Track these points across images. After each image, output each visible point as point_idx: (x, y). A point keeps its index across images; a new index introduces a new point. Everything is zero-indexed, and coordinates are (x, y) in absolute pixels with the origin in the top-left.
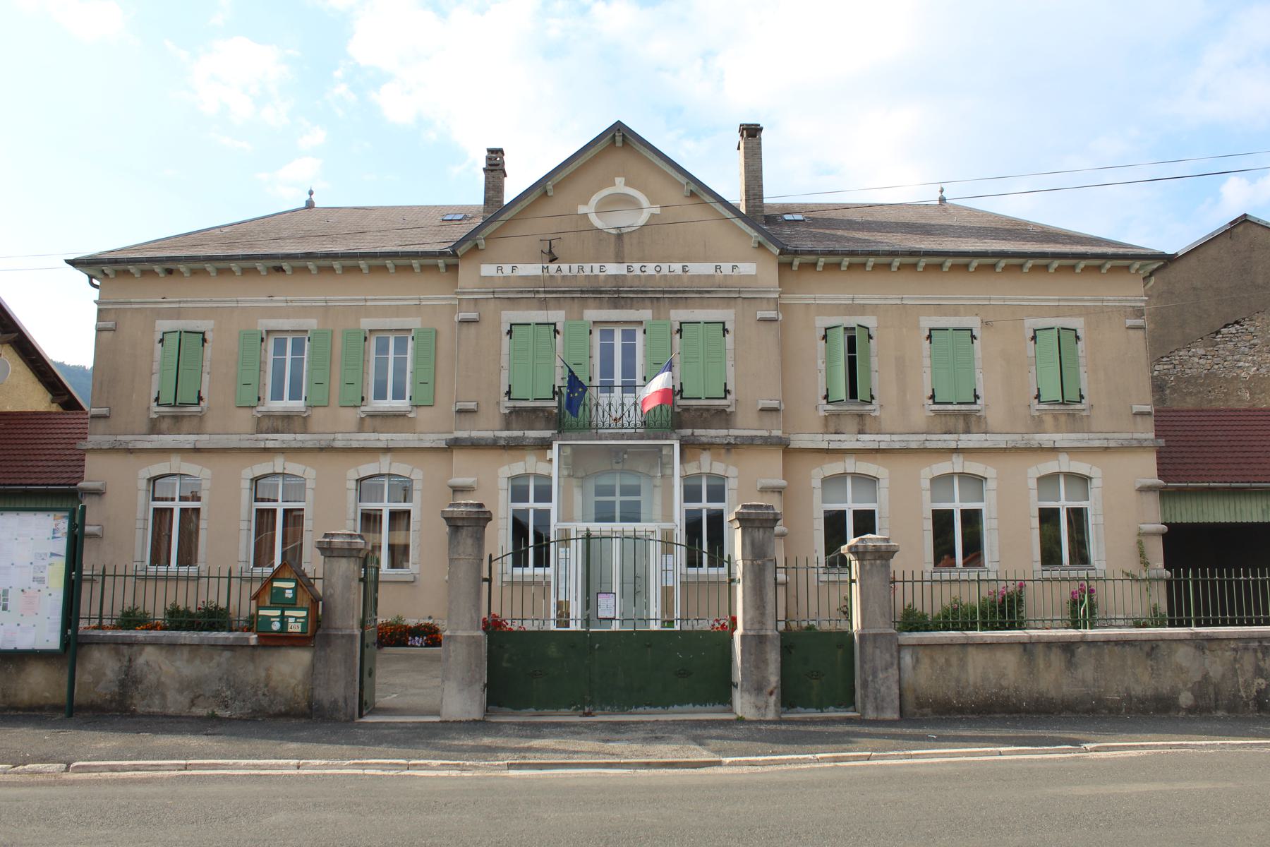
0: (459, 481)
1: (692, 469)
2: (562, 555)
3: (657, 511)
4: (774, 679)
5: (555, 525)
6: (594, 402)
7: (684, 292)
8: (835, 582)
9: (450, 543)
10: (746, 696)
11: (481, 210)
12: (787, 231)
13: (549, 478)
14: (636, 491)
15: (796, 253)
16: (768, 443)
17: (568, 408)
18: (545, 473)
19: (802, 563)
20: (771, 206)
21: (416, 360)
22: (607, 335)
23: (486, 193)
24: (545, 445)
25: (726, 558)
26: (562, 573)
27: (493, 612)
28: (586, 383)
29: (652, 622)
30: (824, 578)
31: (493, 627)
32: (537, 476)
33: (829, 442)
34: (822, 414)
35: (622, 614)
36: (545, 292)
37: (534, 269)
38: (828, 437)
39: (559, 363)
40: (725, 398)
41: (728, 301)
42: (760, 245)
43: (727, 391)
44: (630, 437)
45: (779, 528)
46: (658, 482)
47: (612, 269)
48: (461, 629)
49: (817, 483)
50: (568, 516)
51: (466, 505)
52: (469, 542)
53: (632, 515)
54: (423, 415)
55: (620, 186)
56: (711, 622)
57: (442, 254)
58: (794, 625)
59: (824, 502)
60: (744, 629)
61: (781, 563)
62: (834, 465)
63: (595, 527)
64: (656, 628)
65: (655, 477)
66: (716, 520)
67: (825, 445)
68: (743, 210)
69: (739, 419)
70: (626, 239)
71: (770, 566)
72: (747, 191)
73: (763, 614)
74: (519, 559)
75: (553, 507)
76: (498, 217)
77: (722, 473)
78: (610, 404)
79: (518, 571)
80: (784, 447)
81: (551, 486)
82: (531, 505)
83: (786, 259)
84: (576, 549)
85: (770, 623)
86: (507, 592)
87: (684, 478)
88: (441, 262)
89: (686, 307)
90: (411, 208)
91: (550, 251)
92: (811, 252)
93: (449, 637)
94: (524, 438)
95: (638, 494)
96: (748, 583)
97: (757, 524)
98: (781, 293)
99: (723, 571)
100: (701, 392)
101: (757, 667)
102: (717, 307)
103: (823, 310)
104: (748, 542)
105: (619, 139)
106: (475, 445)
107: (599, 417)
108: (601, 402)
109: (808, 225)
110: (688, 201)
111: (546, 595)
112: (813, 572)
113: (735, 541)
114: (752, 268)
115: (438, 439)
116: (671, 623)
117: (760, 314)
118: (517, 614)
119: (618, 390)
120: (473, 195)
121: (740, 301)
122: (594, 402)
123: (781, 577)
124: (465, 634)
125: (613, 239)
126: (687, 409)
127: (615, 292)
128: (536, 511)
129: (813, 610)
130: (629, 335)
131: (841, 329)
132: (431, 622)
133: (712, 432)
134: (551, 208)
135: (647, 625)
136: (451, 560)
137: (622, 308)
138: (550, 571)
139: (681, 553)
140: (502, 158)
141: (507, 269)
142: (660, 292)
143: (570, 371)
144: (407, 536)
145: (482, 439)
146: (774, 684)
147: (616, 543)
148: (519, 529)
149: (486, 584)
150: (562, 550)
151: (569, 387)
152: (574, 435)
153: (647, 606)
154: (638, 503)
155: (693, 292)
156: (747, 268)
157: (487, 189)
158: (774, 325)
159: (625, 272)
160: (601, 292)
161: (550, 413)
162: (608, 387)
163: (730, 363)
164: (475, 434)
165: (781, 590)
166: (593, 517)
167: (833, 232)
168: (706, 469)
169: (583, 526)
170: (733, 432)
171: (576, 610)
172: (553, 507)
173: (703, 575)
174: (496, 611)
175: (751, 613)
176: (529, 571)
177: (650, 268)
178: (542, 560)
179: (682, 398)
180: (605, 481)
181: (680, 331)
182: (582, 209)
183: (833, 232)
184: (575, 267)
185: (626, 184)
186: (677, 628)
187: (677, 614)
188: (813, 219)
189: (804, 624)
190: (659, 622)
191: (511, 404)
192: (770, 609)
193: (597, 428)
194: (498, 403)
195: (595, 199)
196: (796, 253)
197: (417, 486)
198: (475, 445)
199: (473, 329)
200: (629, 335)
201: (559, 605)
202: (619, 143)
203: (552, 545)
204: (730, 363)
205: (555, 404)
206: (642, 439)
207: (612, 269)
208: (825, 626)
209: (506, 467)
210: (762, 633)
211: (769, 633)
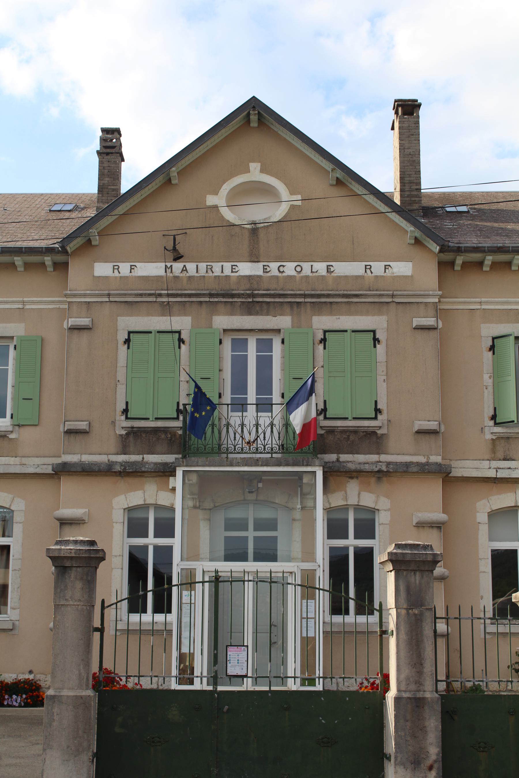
0: (67, 512)
1: (337, 500)
2: (186, 599)
3: (297, 549)
4: (434, 751)
5: (178, 565)
6: (224, 422)
7: (328, 296)
8: (504, 634)
9: (56, 588)
10: (401, 770)
11: (95, 199)
12: (448, 224)
13: (172, 509)
14: (272, 525)
15: (459, 250)
16: (425, 470)
17: (194, 428)
18: (167, 503)
19: (466, 613)
20: (431, 196)
21: (19, 372)
22: (240, 345)
23: (99, 179)
24: (168, 471)
25: (376, 606)
26: (185, 620)
27: (105, 666)
28: (215, 400)
29: (290, 681)
30: (492, 629)
31: (104, 683)
32: (158, 507)
33: (497, 469)
34: (489, 436)
35: (255, 670)
36: (168, 295)
37: (154, 269)
38: (495, 464)
39: (184, 377)
40: (376, 418)
41: (379, 306)
42: (417, 242)
43: (378, 411)
44: (266, 463)
45: (439, 570)
46: (297, 515)
47: (246, 269)
48: (68, 687)
49: (482, 517)
50: (194, 555)
51: (76, 542)
52: (79, 585)
53: (267, 553)
54: (27, 436)
55: (255, 173)
56: (359, 680)
57: (49, 250)
58: (456, 685)
59: (491, 539)
60: (399, 690)
61: (441, 612)
62: (503, 496)
63: (226, 567)
64: (294, 688)
65: (293, 509)
66: (365, 557)
67: (492, 474)
68: (397, 200)
69: (392, 443)
70: (262, 235)
71: (428, 617)
72: (402, 178)
73: (420, 673)
74: (136, 605)
75: (176, 543)
76: (116, 207)
77: (371, 505)
78: (242, 425)
79: (135, 618)
80: (445, 475)
81: (174, 519)
82: (151, 540)
83: (447, 257)
84: (202, 595)
85: (429, 685)
86: (122, 641)
87: (328, 510)
88: (48, 260)
89: (331, 314)
90: (13, 196)
91: (175, 249)
92: (476, 249)
93: (53, 697)
94: (143, 463)
95: (275, 529)
96: (403, 636)
97: (413, 566)
98: (441, 297)
99: (374, 619)
100: (347, 409)
101: (414, 736)
102: (367, 313)
103: (489, 316)
104: (402, 587)
105: (254, 118)
106: (87, 471)
107: (229, 440)
108: (232, 422)
109: (474, 218)
110: (335, 192)
111: (166, 648)
112: (479, 625)
113: (387, 586)
114: (406, 268)
115: (42, 464)
116: (312, 682)
117: (417, 322)
118: (133, 671)
119: (252, 409)
120: (83, 180)
121: (393, 306)
122: (224, 422)
123: (441, 627)
124: (71, 693)
125: (247, 234)
126: (331, 431)
127: (249, 296)
128: (156, 548)
129: (480, 665)
130: (265, 346)
131: (512, 338)
132: (31, 677)
133: (361, 458)
134: (177, 198)
135: (284, 684)
136: (57, 607)
137: (257, 314)
138: (172, 617)
139: (323, 599)
140: (118, 140)
141: (125, 268)
142: (301, 296)
143: (197, 386)
144: (6, 575)
145: (95, 464)
146: (433, 757)
147: (249, 587)
148: (136, 566)
149: (97, 635)
150: (185, 593)
151: (193, 406)
152: (201, 460)
153: (284, 662)
154: (276, 538)
155: (339, 296)
156: (402, 268)
157: (101, 175)
158: (432, 333)
159: (260, 272)
160: (233, 296)
161: (174, 434)
162: (240, 405)
163: (381, 378)
164: (86, 458)
165: (441, 643)
166: (222, 553)
167: (502, 225)
168: (353, 500)
169: (211, 566)
170: (384, 458)
171: (201, 665)
172: (176, 543)
173: (350, 624)
174: (108, 665)
175: (406, 672)
176: (147, 617)
177: (290, 269)
178: (163, 605)
179: (325, 418)
180: (236, 513)
181: (324, 341)
182: (211, 200)
183: (502, 225)
184: (203, 266)
185: (262, 171)
186: (319, 687)
187: (319, 672)
188: (479, 210)
189: (469, 685)
190: (298, 681)
191: (129, 424)
192: (428, 667)
193: (227, 452)
194: (114, 423)
195: (226, 188)
196: (459, 250)
197: (18, 517)
198: (87, 471)
199: (85, 336)
200: (265, 346)
201: (182, 657)
202: (254, 124)
203: (175, 590)
204: (381, 378)
205: (179, 424)
206: (279, 465)
207: (246, 269)
208: (494, 687)
209: (122, 497)
210: (420, 695)
211: (428, 695)
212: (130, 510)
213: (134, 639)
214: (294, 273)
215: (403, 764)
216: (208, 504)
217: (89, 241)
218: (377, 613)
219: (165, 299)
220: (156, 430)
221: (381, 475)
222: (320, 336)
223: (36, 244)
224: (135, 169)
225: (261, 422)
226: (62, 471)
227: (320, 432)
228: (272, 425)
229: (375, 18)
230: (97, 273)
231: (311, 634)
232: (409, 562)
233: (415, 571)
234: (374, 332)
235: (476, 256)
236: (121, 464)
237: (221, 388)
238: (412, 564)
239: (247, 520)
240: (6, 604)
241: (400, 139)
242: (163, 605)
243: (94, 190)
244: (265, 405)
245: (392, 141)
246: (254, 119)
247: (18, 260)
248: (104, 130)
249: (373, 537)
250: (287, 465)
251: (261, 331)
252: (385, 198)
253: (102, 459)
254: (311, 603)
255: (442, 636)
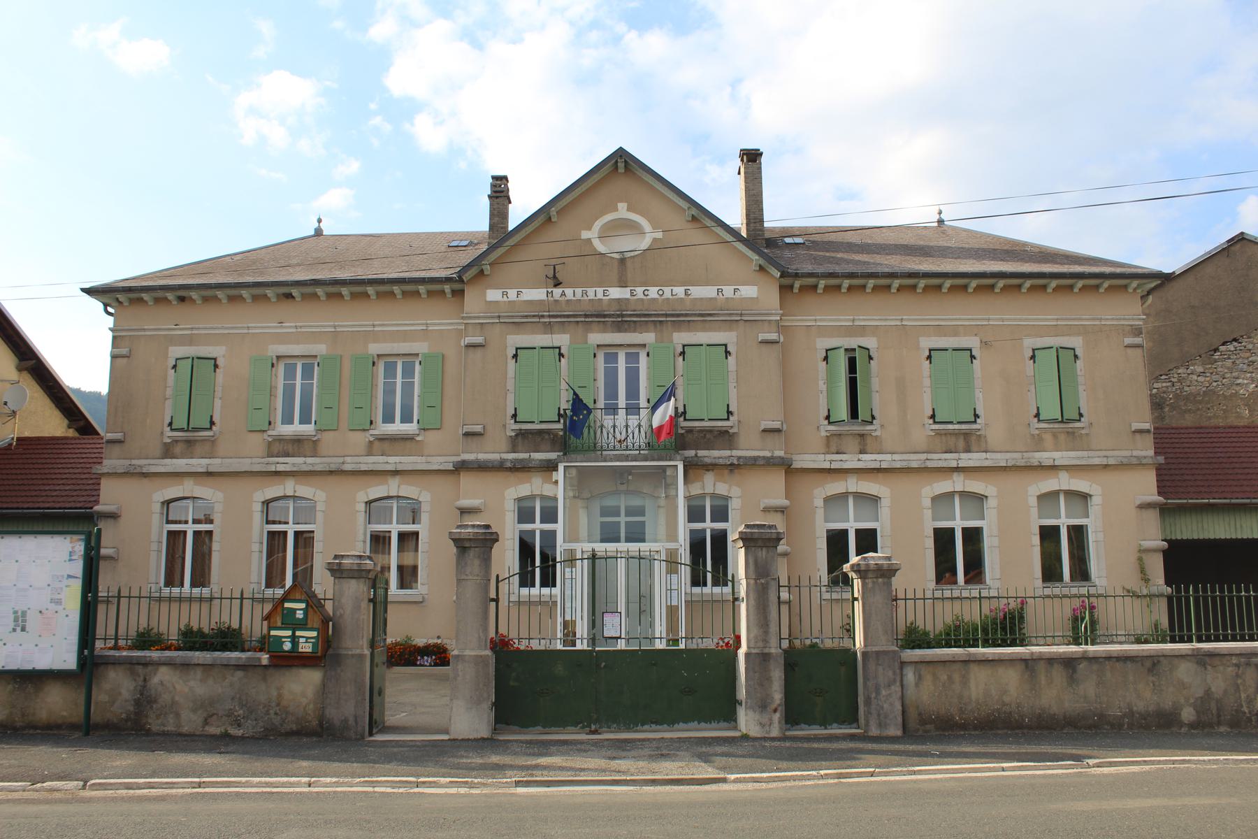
0: (466, 502)
1: (696, 489)
2: (568, 575)
3: (662, 531)
4: (778, 697)
5: (561, 546)
6: (598, 424)
7: (686, 315)
8: (837, 600)
9: (458, 563)
10: (751, 713)
12: (787, 254)
13: (555, 499)
14: (641, 511)
15: (796, 276)
18: (551, 494)
19: (805, 582)
20: (772, 230)
21: (424, 384)
22: (611, 358)
24: (551, 467)
26: (568, 592)
28: (591, 406)
29: (658, 641)
30: (827, 596)
31: (501, 646)
32: (543, 497)
34: (824, 434)
36: (550, 316)
37: (538, 294)
38: (829, 457)
39: (564, 386)
41: (729, 324)
42: (761, 268)
43: (729, 413)
44: (635, 459)
45: (782, 548)
46: (662, 502)
47: (616, 293)
48: (470, 649)
49: (819, 502)
50: (574, 537)
51: (473, 526)
52: (477, 562)
53: (636, 535)
54: (431, 437)
55: (622, 211)
56: (716, 641)
57: (448, 280)
59: (826, 521)
61: (784, 582)
63: (601, 548)
64: (661, 647)
66: (720, 540)
67: (826, 465)
68: (744, 234)
69: (742, 440)
70: (629, 264)
71: (773, 585)
73: (766, 633)
74: (526, 581)
75: (559, 527)
76: (504, 243)
78: (614, 426)
79: (525, 591)
80: (787, 467)
82: (538, 526)
83: (787, 281)
85: (774, 642)
86: (514, 611)
87: (688, 498)
88: (447, 288)
89: (689, 330)
91: (555, 277)
93: (457, 656)
94: (530, 460)
96: (752, 602)
97: (760, 543)
98: (782, 315)
99: (727, 590)
100: (703, 413)
101: (761, 685)
102: (719, 330)
104: (751, 561)
105: (621, 165)
107: (604, 439)
109: (808, 248)
110: (690, 225)
111: (552, 615)
112: (815, 591)
113: (738, 560)
114: (753, 291)
115: (445, 462)
116: (676, 641)
117: (762, 337)
118: (524, 634)
119: (622, 413)
120: (478, 221)
122: (598, 424)
123: (784, 595)
124: (473, 653)
125: (616, 264)
126: (690, 431)
127: (618, 316)
128: (542, 532)
130: (632, 358)
131: (842, 350)
133: (715, 453)
135: (652, 643)
136: (459, 581)
137: (626, 331)
138: (556, 591)
139: (685, 573)
141: (512, 294)
142: (662, 315)
143: (575, 393)
147: (622, 564)
148: (526, 549)
149: (493, 604)
152: (579, 457)
153: (652, 625)
156: (749, 291)
158: (775, 346)
159: (628, 296)
160: (605, 316)
161: (556, 435)
162: (612, 409)
163: (732, 385)
164: (482, 456)
165: (784, 608)
166: (599, 537)
168: (709, 490)
169: (588, 547)
170: (736, 453)
171: (582, 629)
172: (559, 527)
174: (503, 630)
175: (755, 631)
176: (535, 591)
177: (653, 292)
178: (549, 581)
180: (610, 502)
181: (683, 353)
182: (585, 235)
184: (579, 291)
185: (629, 209)
186: (682, 646)
188: (813, 242)
189: (808, 642)
190: (664, 641)
192: (773, 628)
193: (602, 449)
194: (504, 426)
196: (796, 276)
197: (425, 507)
199: (479, 351)
200: (632, 358)
202: (621, 170)
204: (732, 385)
205: (560, 426)
207: (616, 293)
208: (828, 644)
210: (766, 651)
211: (773, 651)
212: (519, 500)
213: (524, 609)
214: (656, 296)
215: (752, 708)
216: (586, 494)
217: (482, 271)
218: (730, 584)
219: (547, 320)
220: (540, 432)
221: (733, 467)
222: (680, 349)
223: (437, 275)
224: (518, 213)
225: (630, 423)
226: (462, 467)
227: (681, 431)
228: (639, 426)
229: (735, 83)
230: (488, 299)
231: (674, 603)
232: (756, 540)
233: (761, 547)
234: (726, 345)
235: (811, 281)
236: (511, 461)
237: (596, 395)
238: (761, 542)
239: (619, 507)
240: (416, 581)
241: (746, 182)
242: (549, 581)
243: (486, 228)
244: (633, 409)
245: (738, 185)
246: (621, 165)
247: (422, 289)
248: (493, 178)
249: (726, 520)
250: (653, 460)
251: (629, 346)
252: (734, 232)
253: (496, 457)
254: (674, 577)
255: (785, 603)
